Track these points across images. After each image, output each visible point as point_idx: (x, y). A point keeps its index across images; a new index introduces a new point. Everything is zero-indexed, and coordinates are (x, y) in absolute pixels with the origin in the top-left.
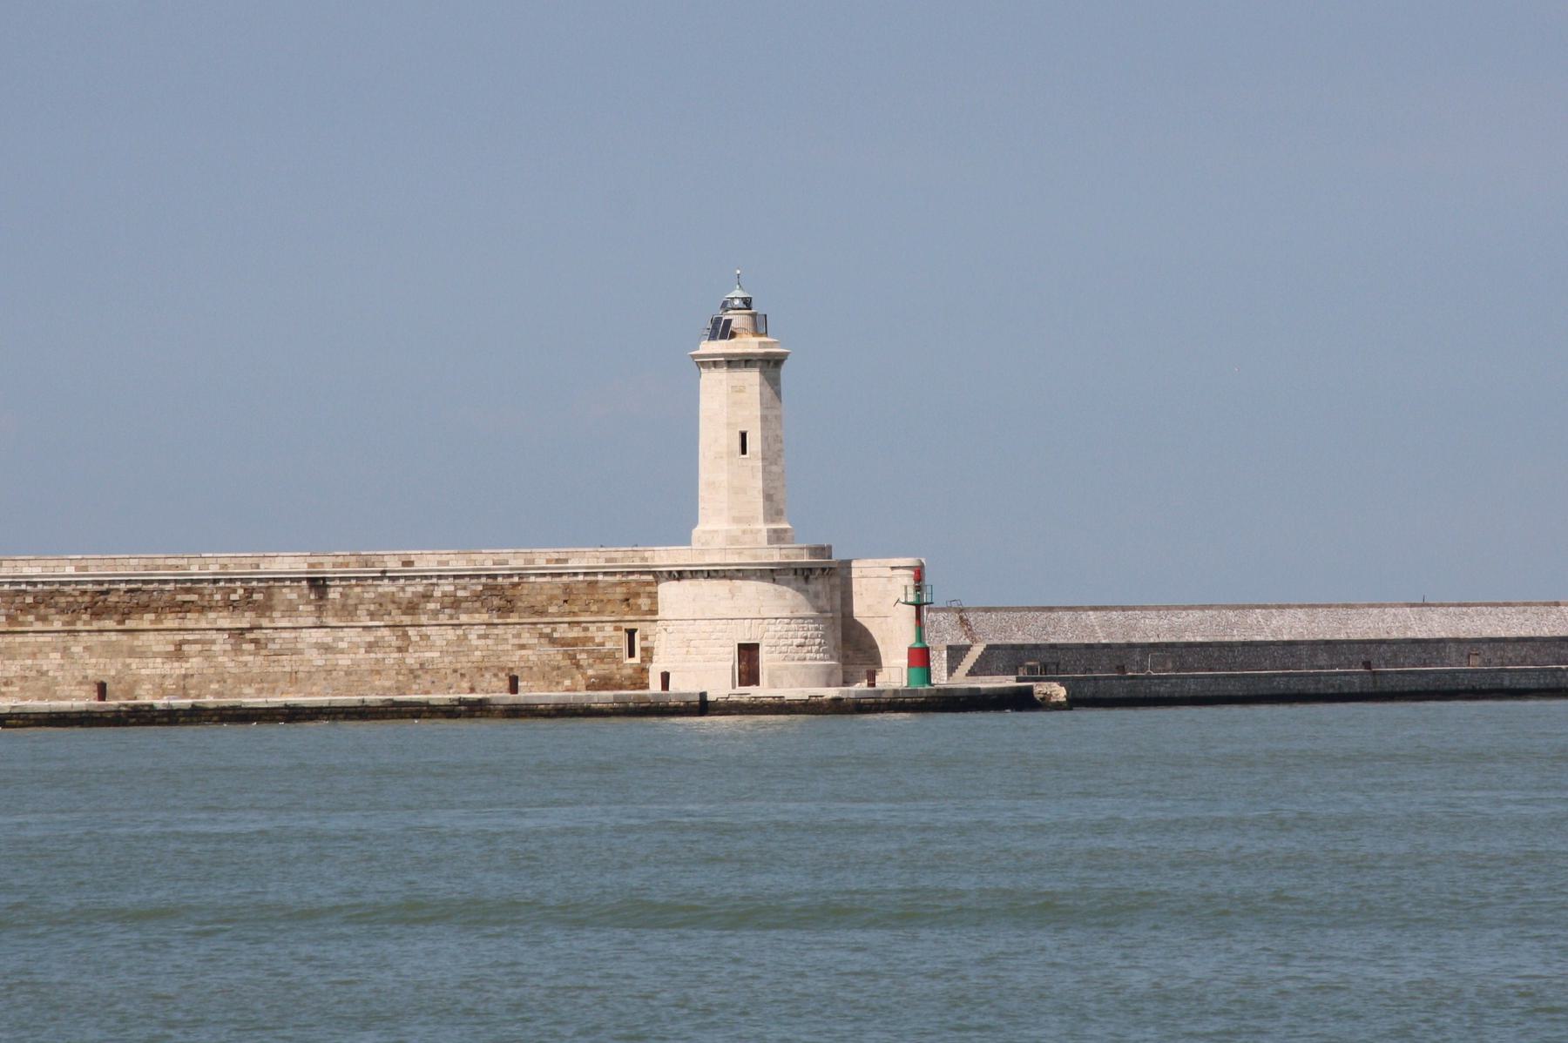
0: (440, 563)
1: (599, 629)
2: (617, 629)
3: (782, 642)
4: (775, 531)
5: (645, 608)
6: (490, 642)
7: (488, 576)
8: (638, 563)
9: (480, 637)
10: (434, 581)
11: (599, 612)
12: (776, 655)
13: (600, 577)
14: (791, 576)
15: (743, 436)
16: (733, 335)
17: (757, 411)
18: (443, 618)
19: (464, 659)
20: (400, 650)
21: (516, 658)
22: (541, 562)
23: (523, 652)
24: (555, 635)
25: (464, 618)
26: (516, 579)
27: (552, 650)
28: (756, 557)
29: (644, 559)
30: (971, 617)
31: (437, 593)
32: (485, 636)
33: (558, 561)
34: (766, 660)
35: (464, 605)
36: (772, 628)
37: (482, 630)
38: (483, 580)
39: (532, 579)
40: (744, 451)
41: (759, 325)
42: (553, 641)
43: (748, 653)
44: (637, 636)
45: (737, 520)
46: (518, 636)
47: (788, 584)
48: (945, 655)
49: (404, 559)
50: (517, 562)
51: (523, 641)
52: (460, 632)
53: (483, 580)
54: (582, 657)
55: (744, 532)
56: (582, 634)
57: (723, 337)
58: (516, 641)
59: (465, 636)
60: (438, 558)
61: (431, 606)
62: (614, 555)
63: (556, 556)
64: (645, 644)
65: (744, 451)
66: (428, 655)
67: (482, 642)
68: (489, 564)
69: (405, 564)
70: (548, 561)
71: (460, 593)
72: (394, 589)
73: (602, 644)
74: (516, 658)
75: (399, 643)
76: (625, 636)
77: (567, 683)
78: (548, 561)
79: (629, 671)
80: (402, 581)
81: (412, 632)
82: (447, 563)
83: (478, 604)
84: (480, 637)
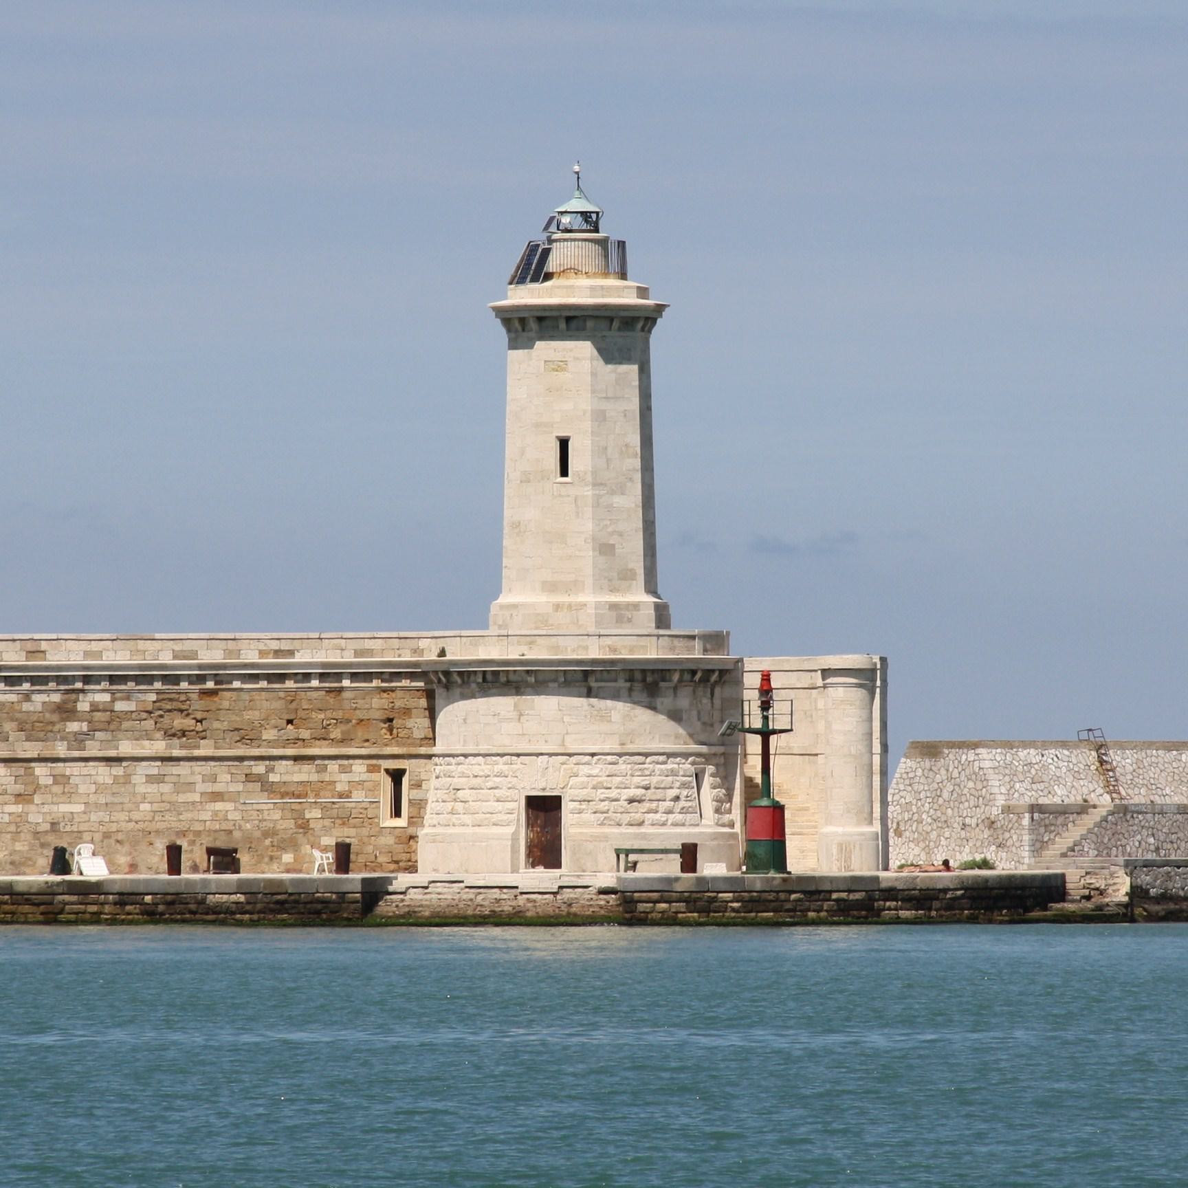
0: (87, 654)
1: (344, 770)
2: (373, 769)
3: (602, 793)
4: (614, 606)
5: (418, 734)
6: (166, 788)
7: (165, 679)
8: (407, 657)
9: (150, 779)
10: (79, 685)
11: (343, 741)
12: (588, 816)
13: (346, 683)
14: (622, 684)
15: (564, 444)
16: (549, 276)
17: (586, 403)
18: (93, 749)
19: (123, 816)
20: (19, 797)
21: (206, 816)
22: (250, 656)
23: (219, 806)
24: (273, 778)
25: (126, 748)
26: (210, 685)
27: (262, 801)
28: (556, 648)
29: (415, 651)
30: (1114, 756)
31: (83, 706)
32: (158, 779)
33: (277, 653)
34: (572, 824)
35: (126, 725)
36: (585, 770)
37: (154, 768)
38: (158, 685)
39: (237, 684)
40: (564, 472)
41: (615, 257)
42: (268, 788)
43: (544, 810)
44: (405, 781)
45: (551, 587)
46: (214, 779)
47: (615, 696)
48: (1026, 821)
49: (30, 646)
50: (212, 655)
51: (218, 787)
52: (118, 770)
53: (158, 685)
54: (313, 814)
55: (557, 607)
56: (314, 777)
57: (535, 279)
58: (209, 788)
59: (128, 776)
60: (84, 646)
61: (73, 727)
62: (369, 644)
63: (275, 645)
64: (416, 794)
65: (564, 472)
66: (64, 808)
67: (152, 788)
68: (166, 659)
69: (31, 653)
70: (262, 653)
71: (120, 706)
72: (13, 698)
73: (348, 795)
74: (206, 816)
75: (19, 788)
76: (388, 782)
77: (288, 858)
78: (262, 653)
79: (389, 840)
80: (26, 686)
81: (40, 770)
82: (99, 654)
83: (149, 724)
84: (150, 779)
